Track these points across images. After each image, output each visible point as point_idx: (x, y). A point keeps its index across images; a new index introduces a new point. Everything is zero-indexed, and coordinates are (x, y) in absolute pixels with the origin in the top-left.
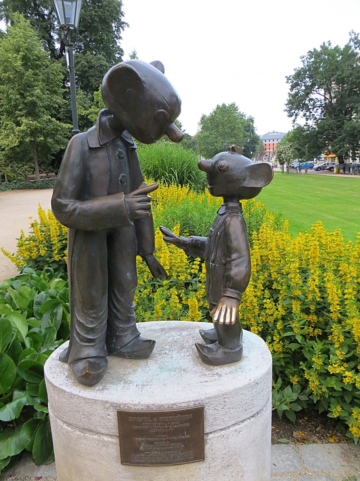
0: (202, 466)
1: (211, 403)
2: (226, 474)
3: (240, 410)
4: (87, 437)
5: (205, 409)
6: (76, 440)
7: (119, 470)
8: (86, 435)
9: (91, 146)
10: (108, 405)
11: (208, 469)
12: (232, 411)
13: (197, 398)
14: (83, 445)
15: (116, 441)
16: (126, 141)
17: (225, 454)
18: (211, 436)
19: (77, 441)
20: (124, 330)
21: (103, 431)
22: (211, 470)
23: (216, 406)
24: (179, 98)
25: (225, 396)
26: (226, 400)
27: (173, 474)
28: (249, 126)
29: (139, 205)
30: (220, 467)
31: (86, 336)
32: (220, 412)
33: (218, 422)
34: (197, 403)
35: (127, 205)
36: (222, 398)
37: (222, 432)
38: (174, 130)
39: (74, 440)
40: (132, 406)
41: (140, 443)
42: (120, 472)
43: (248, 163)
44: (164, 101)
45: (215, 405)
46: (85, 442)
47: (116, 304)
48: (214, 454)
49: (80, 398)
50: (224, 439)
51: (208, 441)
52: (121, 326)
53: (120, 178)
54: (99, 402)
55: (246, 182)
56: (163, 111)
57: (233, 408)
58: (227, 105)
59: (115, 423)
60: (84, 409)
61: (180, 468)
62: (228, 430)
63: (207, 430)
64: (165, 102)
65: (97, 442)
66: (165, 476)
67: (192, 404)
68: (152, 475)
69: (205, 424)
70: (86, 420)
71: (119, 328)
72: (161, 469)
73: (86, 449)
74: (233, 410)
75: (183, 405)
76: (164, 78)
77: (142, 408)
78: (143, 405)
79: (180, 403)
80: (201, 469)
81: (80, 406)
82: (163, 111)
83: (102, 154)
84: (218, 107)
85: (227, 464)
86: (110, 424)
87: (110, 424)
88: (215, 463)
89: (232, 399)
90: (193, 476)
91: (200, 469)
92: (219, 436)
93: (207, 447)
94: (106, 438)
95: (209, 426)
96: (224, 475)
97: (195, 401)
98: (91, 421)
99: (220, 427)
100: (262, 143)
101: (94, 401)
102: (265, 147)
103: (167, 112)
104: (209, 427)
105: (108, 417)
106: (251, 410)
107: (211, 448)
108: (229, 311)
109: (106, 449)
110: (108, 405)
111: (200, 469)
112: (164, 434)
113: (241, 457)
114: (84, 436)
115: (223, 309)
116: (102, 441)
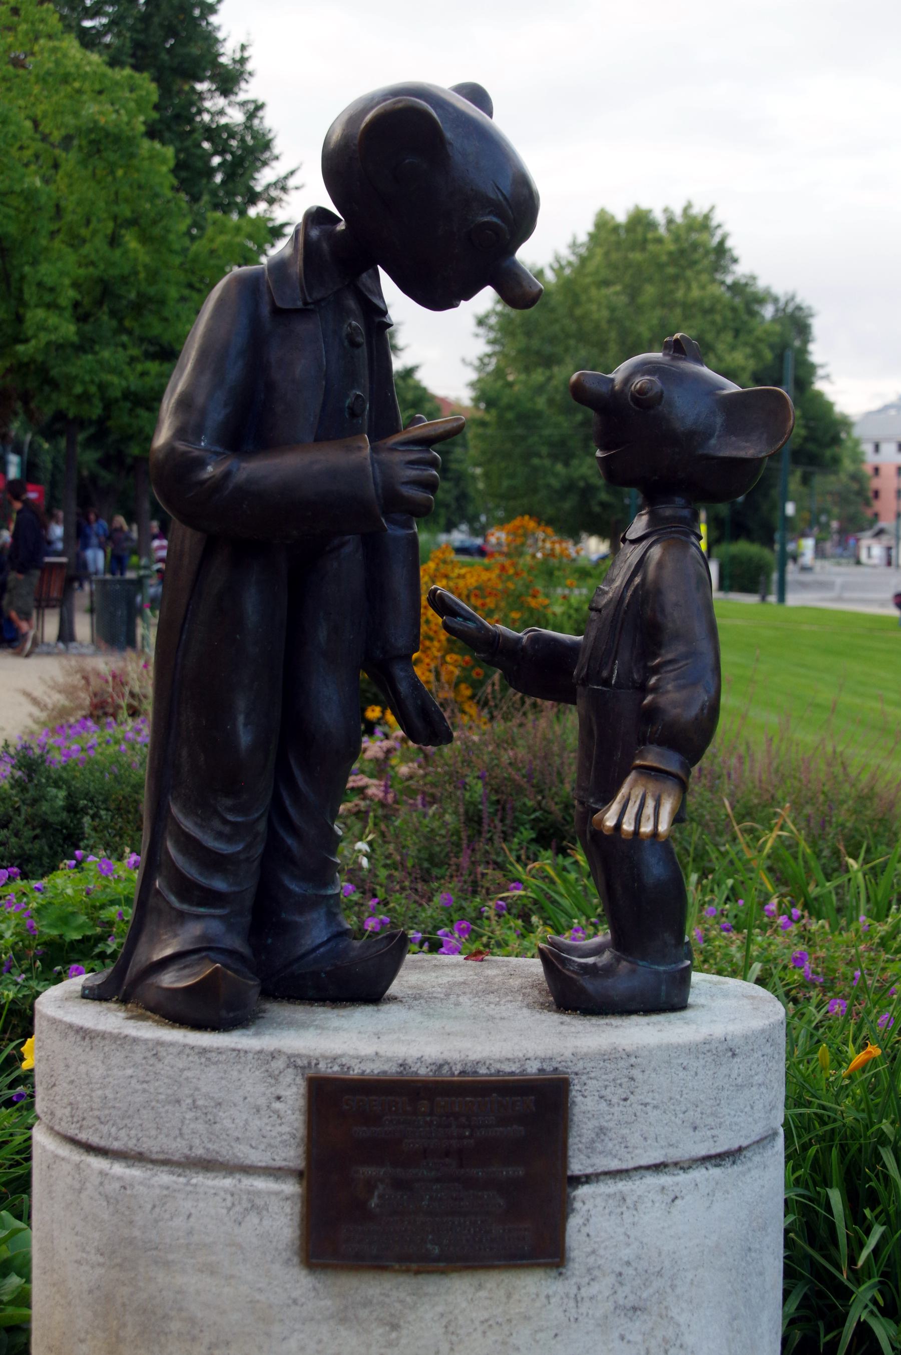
0: (554, 1288)
1: (593, 1075)
2: (629, 1337)
3: (679, 1122)
4: (195, 1185)
5: (575, 1093)
6: (154, 1207)
7: (295, 1294)
8: (194, 1181)
9: (279, 304)
10: (279, 1064)
11: (572, 1304)
12: (654, 1115)
13: (549, 1054)
14: (178, 1222)
15: (291, 1188)
16: (370, 301)
17: (628, 1263)
18: (583, 1191)
19: (157, 1210)
20: (305, 905)
21: (257, 1157)
22: (583, 1309)
23: (606, 1087)
24: (534, 187)
25: (633, 1060)
26: (635, 1072)
27: (464, 1305)
28: (781, 350)
29: (412, 473)
30: (610, 1305)
31: (203, 880)
32: (616, 1110)
33: (610, 1145)
34: (548, 1067)
35: (377, 471)
36: (622, 1064)
37: (622, 1186)
38: (516, 274)
39: (149, 1206)
40: (353, 1063)
41: (370, 1186)
42: (295, 1302)
43: (723, 389)
44: (499, 195)
45: (601, 1083)
46: (188, 1205)
47: (292, 811)
48: (594, 1252)
49: (187, 1051)
50: (624, 1208)
51: (577, 1205)
52: (294, 887)
53: (348, 402)
54: (250, 1056)
55: (713, 442)
56: (495, 220)
57: (656, 1107)
58: (214, 19)
59: (296, 1125)
60: (197, 1089)
61: (488, 1285)
62: (638, 1183)
63: (576, 1167)
64: (504, 203)
65: (229, 1198)
66: (440, 1309)
67: (532, 1068)
68: (398, 1306)
69: (571, 1141)
70: (200, 1127)
71: (289, 892)
72: (432, 1285)
73: (190, 1233)
74: (656, 1112)
75: (507, 1068)
76: (492, 127)
77: (386, 1067)
78: (389, 1060)
79: (500, 1061)
80: (553, 1300)
81: (187, 1079)
82: (495, 220)
83: (304, 328)
84: (604, 224)
85: (632, 1300)
86: (279, 1129)
87: (279, 1129)
88: (594, 1289)
89: (653, 1075)
90: (527, 1318)
91: (548, 1297)
92: (609, 1196)
93: (574, 1222)
94: (261, 1184)
95: (579, 1150)
96: (622, 1338)
97: (543, 1060)
98: (218, 1126)
99: (615, 1165)
100: (858, 458)
101: (235, 1054)
102: (875, 483)
103: (503, 220)
104: (582, 1157)
105: (277, 1105)
106: (714, 1132)
107: (585, 1230)
108: (649, 810)
109: (256, 1221)
110: (279, 1064)
111: (548, 1297)
112: (447, 1154)
113: (679, 1291)
114: (188, 1184)
115: (633, 799)
116: (249, 1193)
